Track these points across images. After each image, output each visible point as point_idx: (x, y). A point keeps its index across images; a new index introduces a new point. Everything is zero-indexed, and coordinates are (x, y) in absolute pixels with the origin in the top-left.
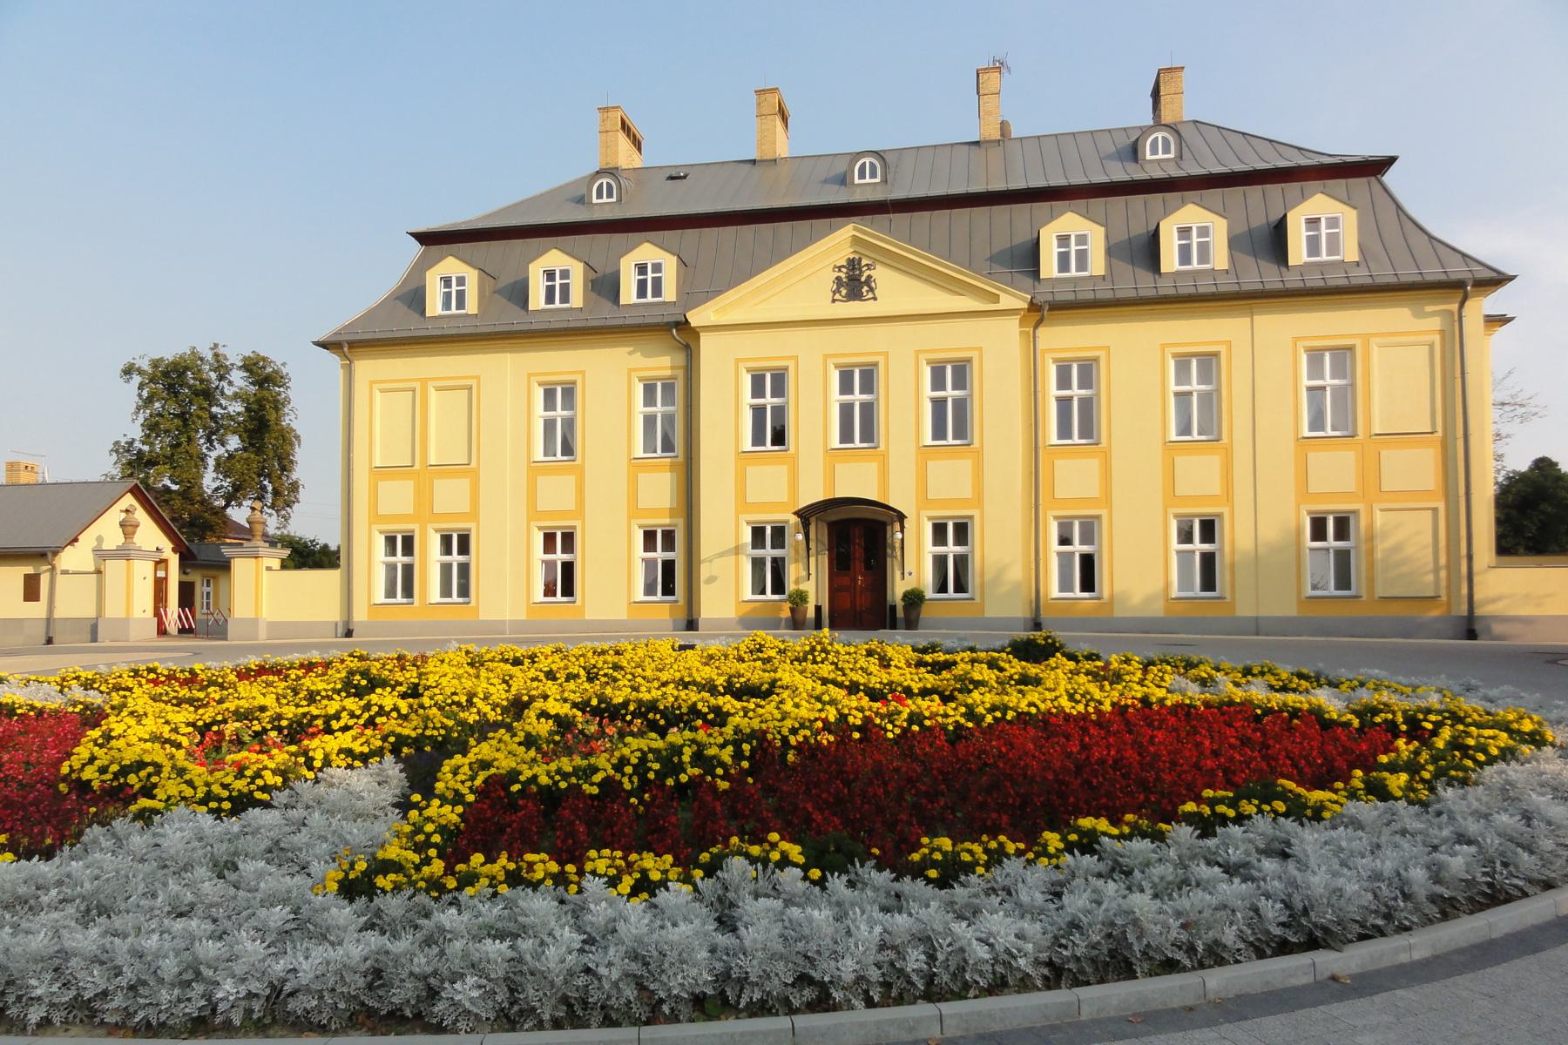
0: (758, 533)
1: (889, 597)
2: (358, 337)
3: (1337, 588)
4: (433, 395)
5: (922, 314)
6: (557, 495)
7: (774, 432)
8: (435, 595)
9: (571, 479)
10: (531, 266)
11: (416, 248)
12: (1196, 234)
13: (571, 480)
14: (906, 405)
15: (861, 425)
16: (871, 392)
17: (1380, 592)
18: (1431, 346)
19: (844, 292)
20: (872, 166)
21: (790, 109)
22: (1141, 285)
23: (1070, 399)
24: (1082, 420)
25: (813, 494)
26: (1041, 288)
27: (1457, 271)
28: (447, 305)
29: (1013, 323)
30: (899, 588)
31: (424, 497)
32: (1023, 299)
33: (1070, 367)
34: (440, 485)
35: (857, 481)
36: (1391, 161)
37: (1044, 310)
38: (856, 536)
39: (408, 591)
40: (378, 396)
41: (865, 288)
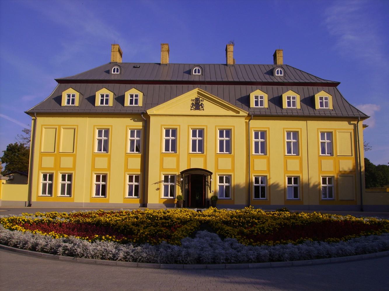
0: (166, 177)
2: (39, 111)
3: (294, 197)
4: (62, 130)
5: (216, 116)
6: (102, 163)
7: (172, 146)
8: (59, 194)
9: (106, 159)
10: (63, 93)
11: (56, 84)
12: (291, 98)
13: (106, 159)
14: (212, 141)
15: (199, 146)
18: (351, 133)
19: (194, 107)
20: (117, 69)
21: (122, 50)
22: (276, 111)
24: (262, 148)
25: (184, 167)
26: (250, 110)
27: (356, 114)
28: (68, 103)
29: (243, 121)
30: (210, 195)
31: (57, 163)
33: (258, 133)
34: (63, 159)
35: (197, 163)
36: (339, 83)
37: (254, 116)
38: (196, 180)
39: (50, 192)
40: (44, 129)
41: (201, 107)
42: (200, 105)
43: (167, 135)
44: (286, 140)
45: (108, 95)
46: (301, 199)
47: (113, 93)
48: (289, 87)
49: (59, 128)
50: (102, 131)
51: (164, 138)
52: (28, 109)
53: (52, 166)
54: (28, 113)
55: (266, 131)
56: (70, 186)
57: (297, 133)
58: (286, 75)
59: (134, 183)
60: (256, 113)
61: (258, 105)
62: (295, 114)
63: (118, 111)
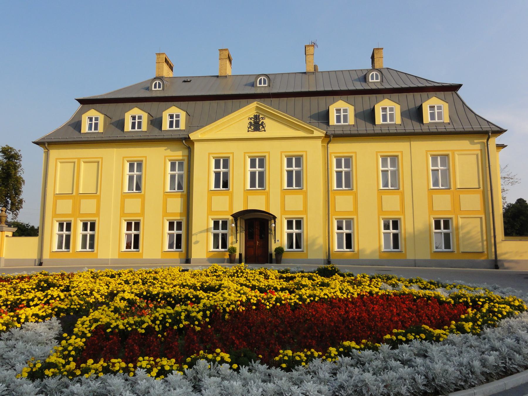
0: (216, 223)
4: (82, 164)
5: (283, 137)
6: (133, 207)
7: (223, 182)
8: (79, 248)
11: (78, 105)
12: (389, 111)
14: (277, 173)
15: (258, 181)
17: (462, 250)
18: (477, 155)
19: (252, 128)
20: (264, 80)
22: (368, 129)
23: (341, 172)
24: (346, 180)
25: (239, 208)
26: (330, 129)
27: (486, 127)
28: (90, 128)
29: (319, 142)
31: (76, 207)
33: (292, 159)
35: (257, 203)
36: (460, 86)
37: (332, 137)
39: (68, 246)
40: (59, 164)
42: (259, 125)
43: (253, 165)
44: (381, 168)
45: (346, 109)
46: (485, 250)
47: (147, 114)
48: (430, 94)
49: (78, 161)
50: (134, 164)
51: (249, 169)
52: (36, 139)
53: (449, 208)
54: (37, 143)
55: (351, 157)
56: (92, 237)
57: (447, 157)
58: (384, 80)
59: (175, 232)
60: (337, 132)
61: (134, 129)
62: (441, 129)
63: (154, 138)
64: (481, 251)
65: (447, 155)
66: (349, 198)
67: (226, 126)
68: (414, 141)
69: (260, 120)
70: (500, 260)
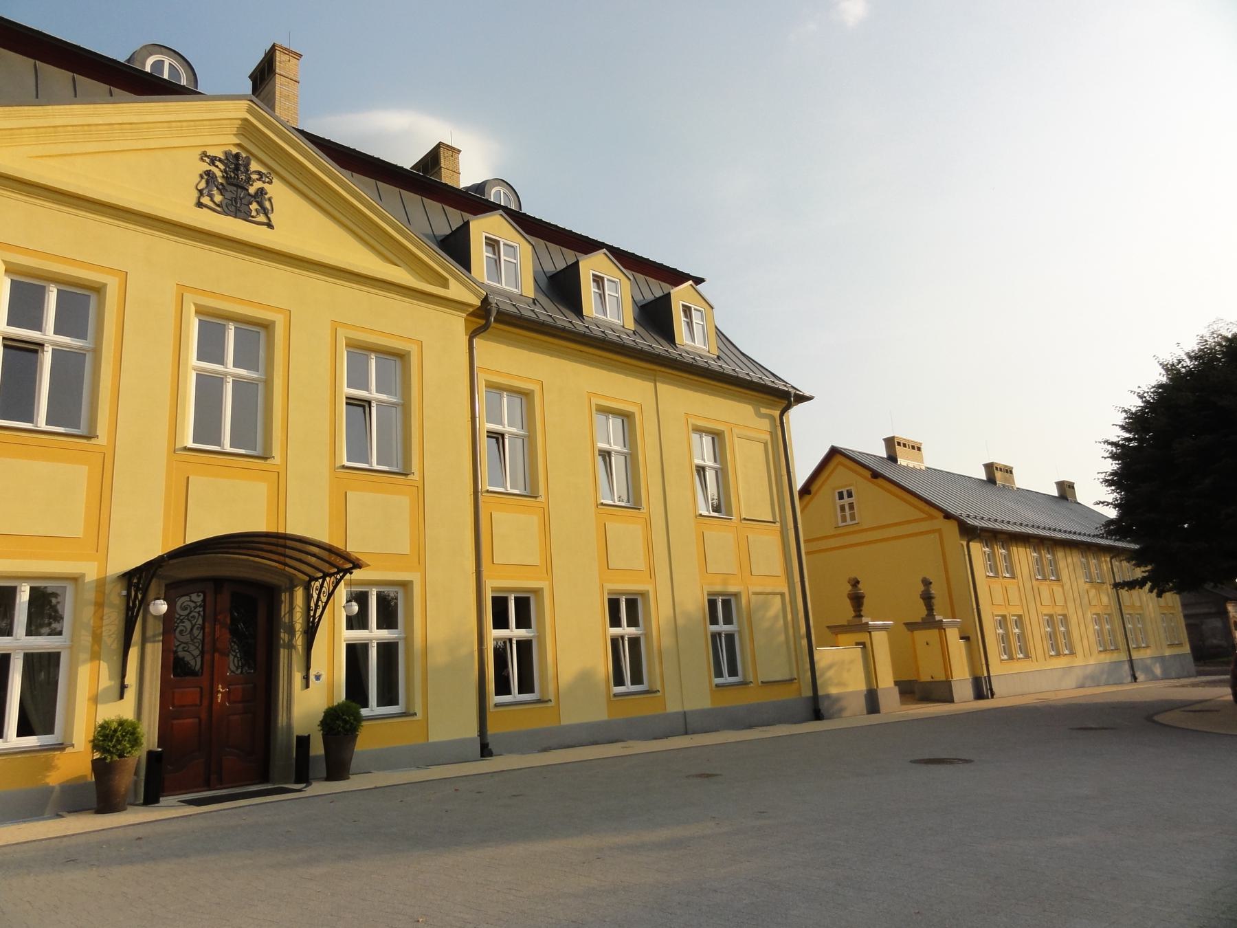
1: (282, 720)
15: (238, 422)
16: (80, 333)
17: (761, 679)
18: (766, 444)
23: (35, 348)
29: (457, 324)
32: (478, 297)
35: (229, 506)
41: (254, 206)
64: (787, 677)
65: (267, 326)
66: (399, 502)
67: (91, 147)
68: (664, 383)
69: (249, 180)
70: (828, 696)
